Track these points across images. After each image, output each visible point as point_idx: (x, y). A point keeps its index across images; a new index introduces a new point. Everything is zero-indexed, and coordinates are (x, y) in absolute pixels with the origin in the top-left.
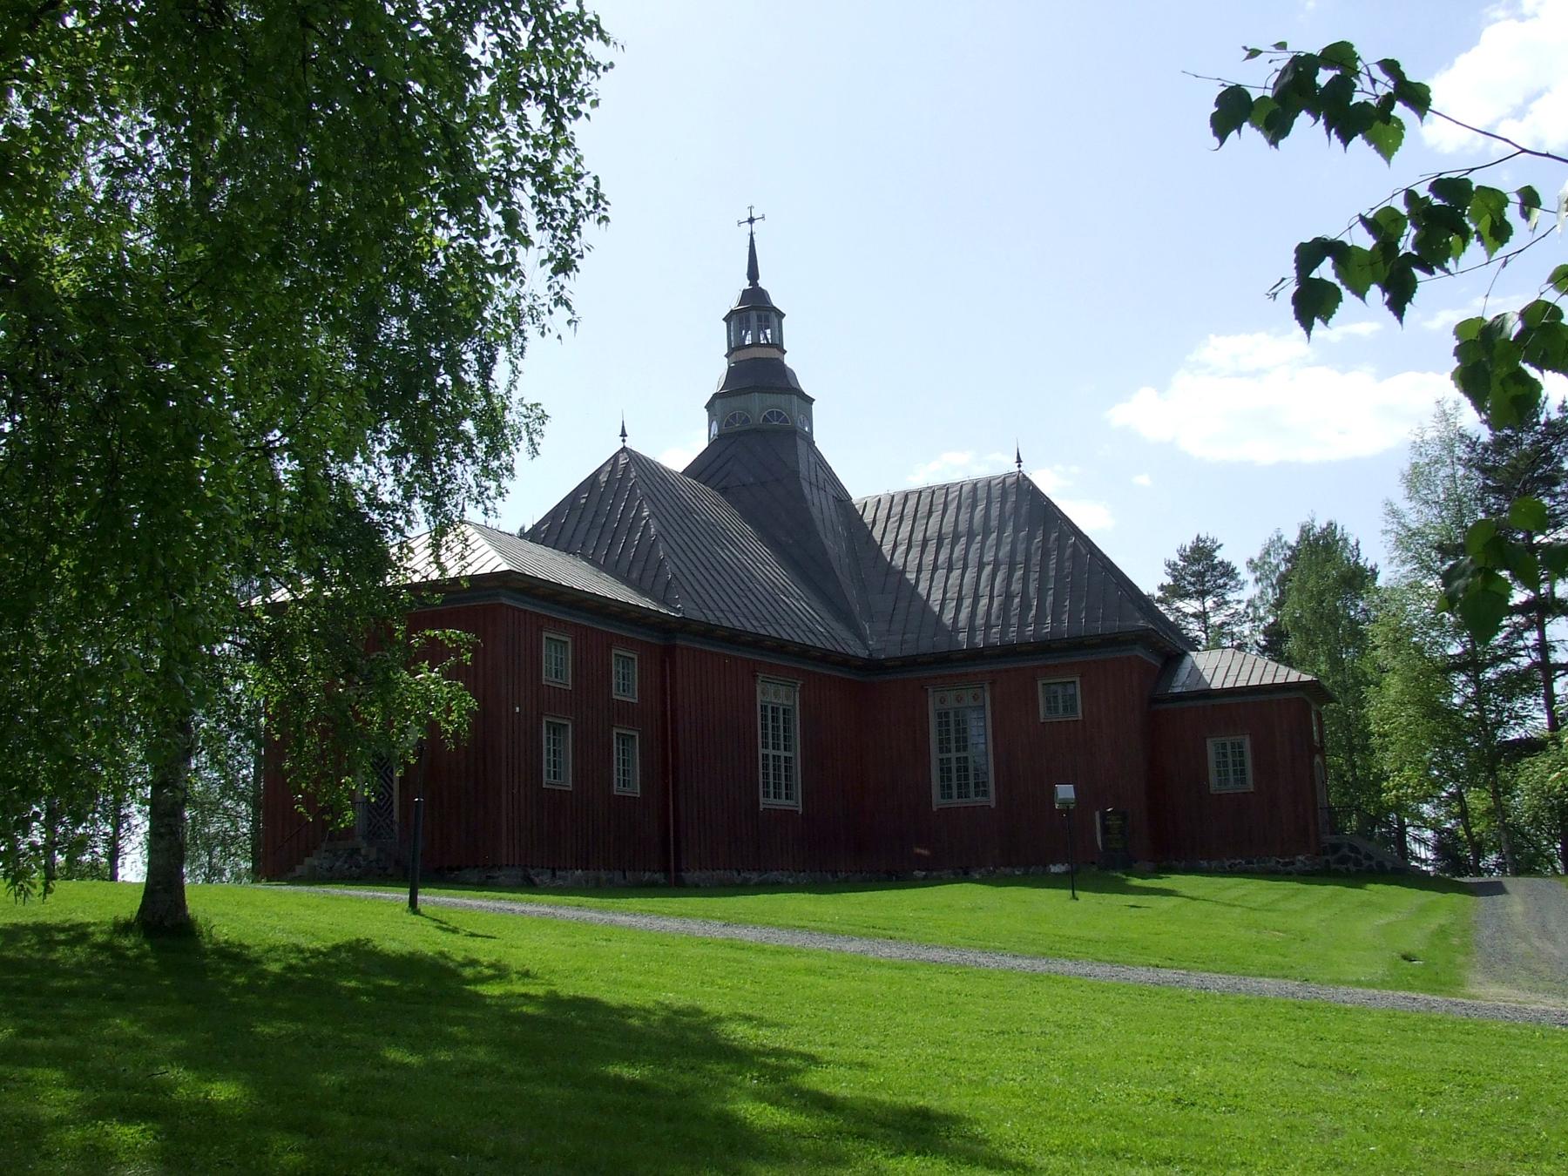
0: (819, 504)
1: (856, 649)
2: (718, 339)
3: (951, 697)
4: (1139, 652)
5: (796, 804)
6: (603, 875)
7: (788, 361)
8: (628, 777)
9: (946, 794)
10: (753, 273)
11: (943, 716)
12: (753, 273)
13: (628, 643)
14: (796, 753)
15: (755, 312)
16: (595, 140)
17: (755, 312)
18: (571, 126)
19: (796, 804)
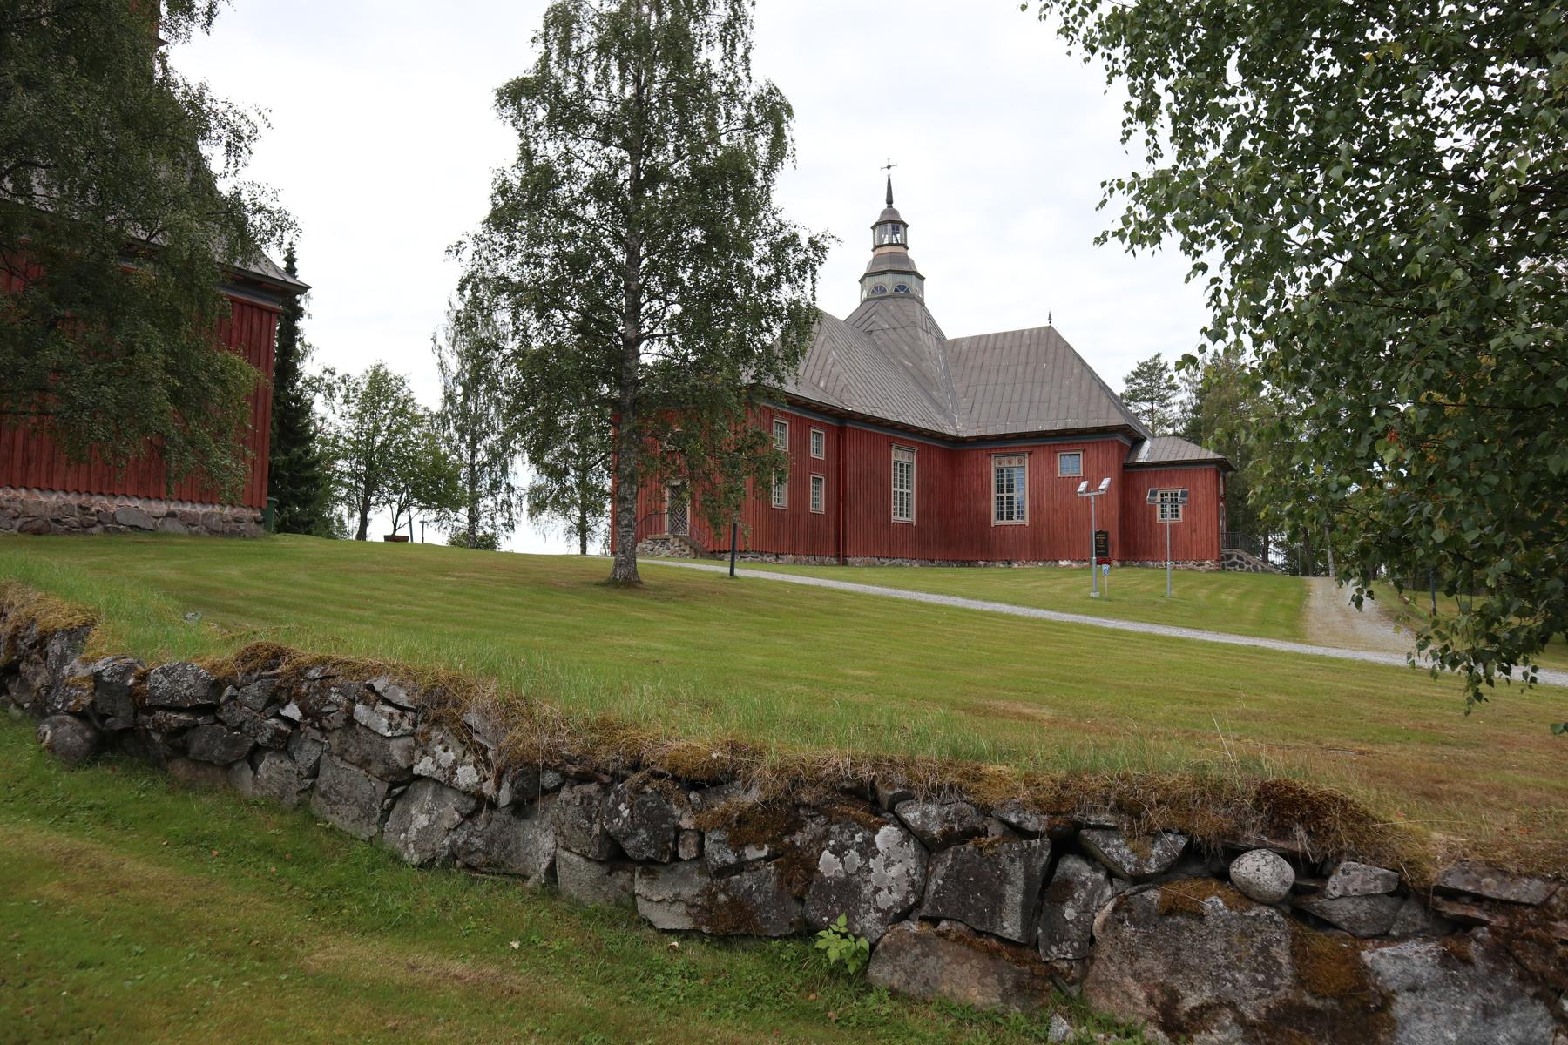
0: (927, 340)
1: (950, 431)
2: (868, 240)
3: (1005, 463)
4: (1120, 438)
5: (912, 519)
6: (804, 558)
7: (910, 253)
8: (818, 501)
9: (1000, 515)
10: (890, 202)
11: (1000, 471)
12: (890, 202)
13: (820, 425)
14: (913, 491)
15: (891, 223)
16: (495, 149)
17: (891, 223)
18: (542, 31)
19: (912, 519)
